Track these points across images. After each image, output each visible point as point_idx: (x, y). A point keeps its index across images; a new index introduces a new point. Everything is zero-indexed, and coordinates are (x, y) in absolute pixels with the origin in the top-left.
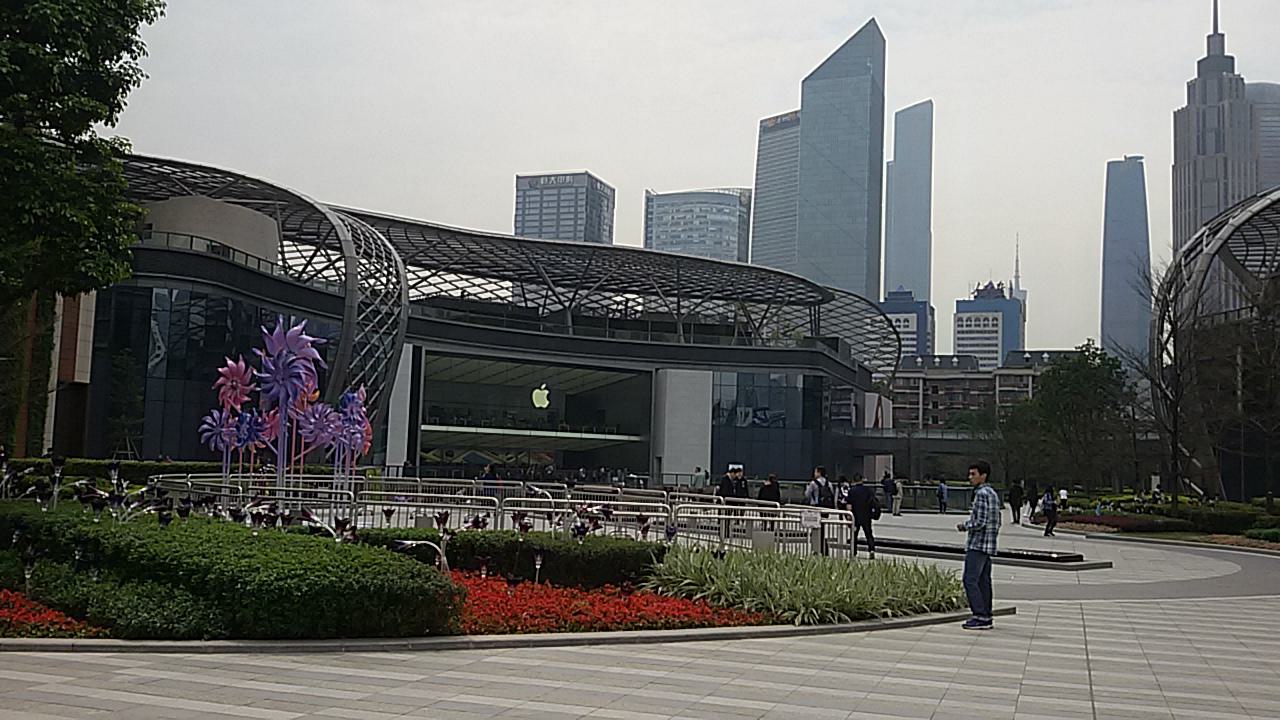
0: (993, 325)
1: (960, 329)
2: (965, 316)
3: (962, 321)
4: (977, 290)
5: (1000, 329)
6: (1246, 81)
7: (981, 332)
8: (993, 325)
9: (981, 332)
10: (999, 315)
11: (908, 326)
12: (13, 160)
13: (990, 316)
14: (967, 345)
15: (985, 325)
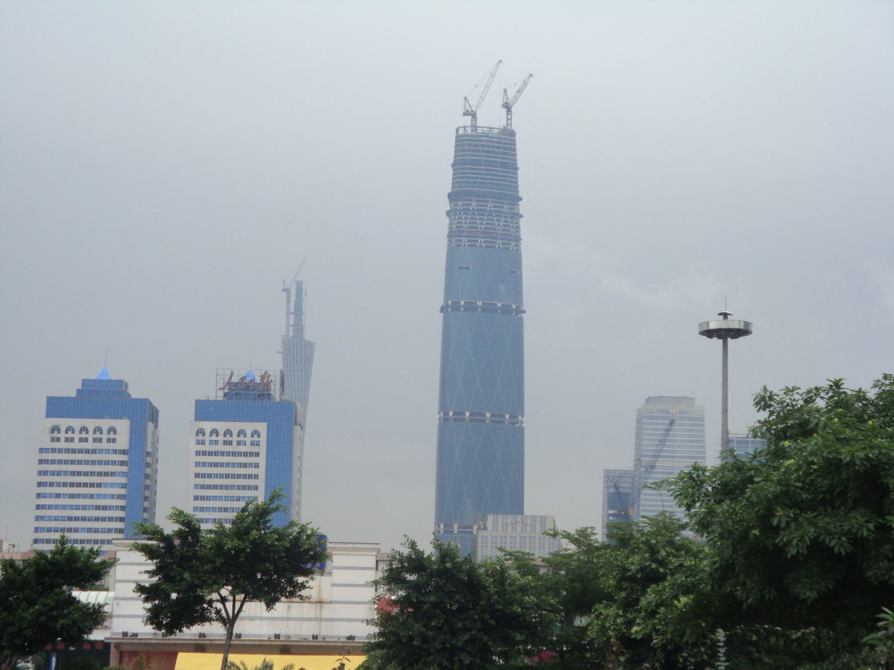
0: (252, 444)
1: (201, 448)
2: (208, 426)
3: (204, 434)
4: (229, 383)
5: (262, 449)
6: (449, 209)
7: (234, 454)
8: (252, 444)
9: (234, 454)
10: (262, 427)
11: (114, 440)
12: (494, 587)
13: (249, 427)
14: (80, 462)
15: (239, 443)
